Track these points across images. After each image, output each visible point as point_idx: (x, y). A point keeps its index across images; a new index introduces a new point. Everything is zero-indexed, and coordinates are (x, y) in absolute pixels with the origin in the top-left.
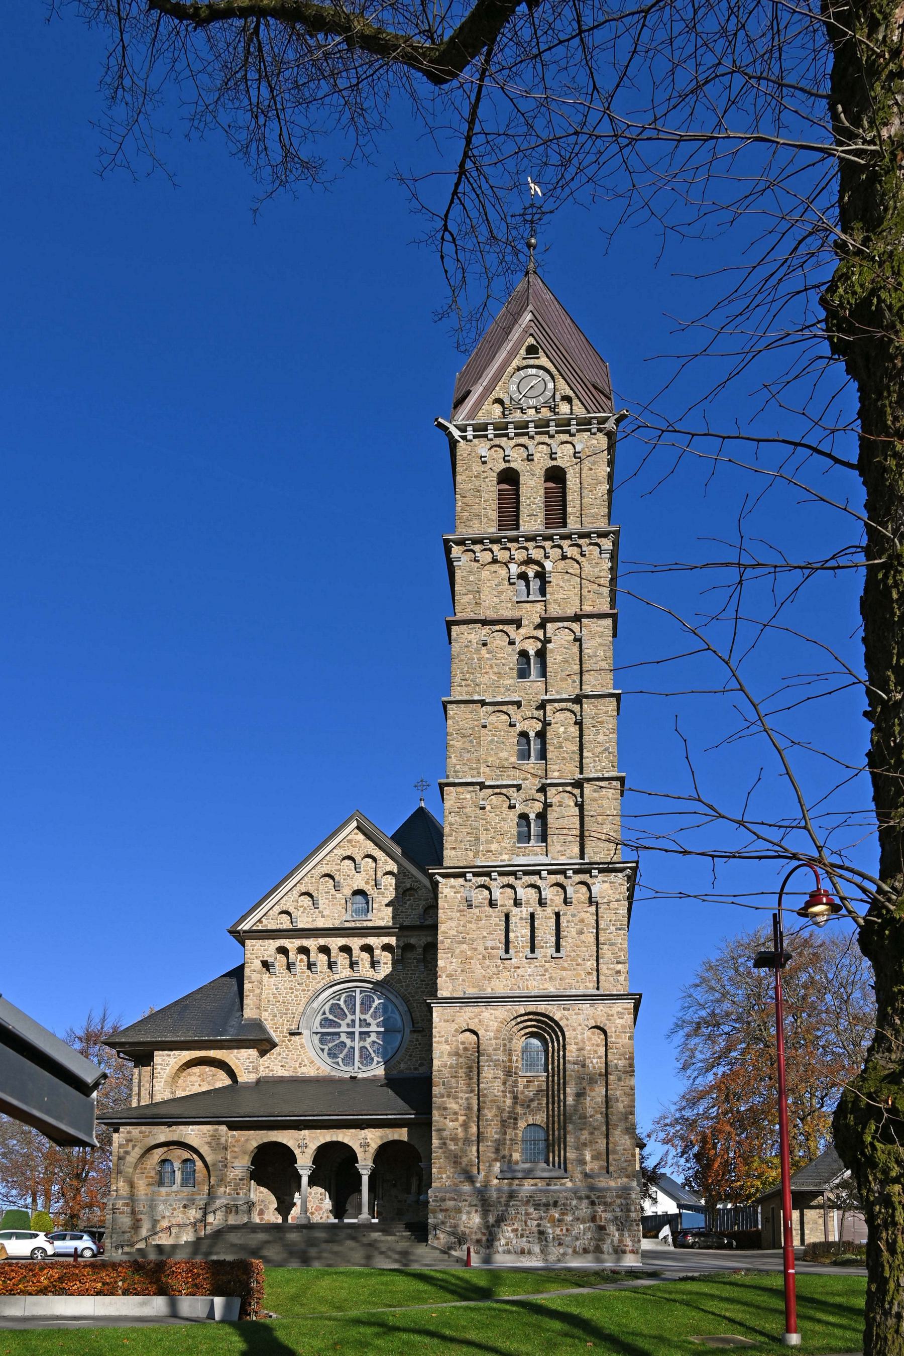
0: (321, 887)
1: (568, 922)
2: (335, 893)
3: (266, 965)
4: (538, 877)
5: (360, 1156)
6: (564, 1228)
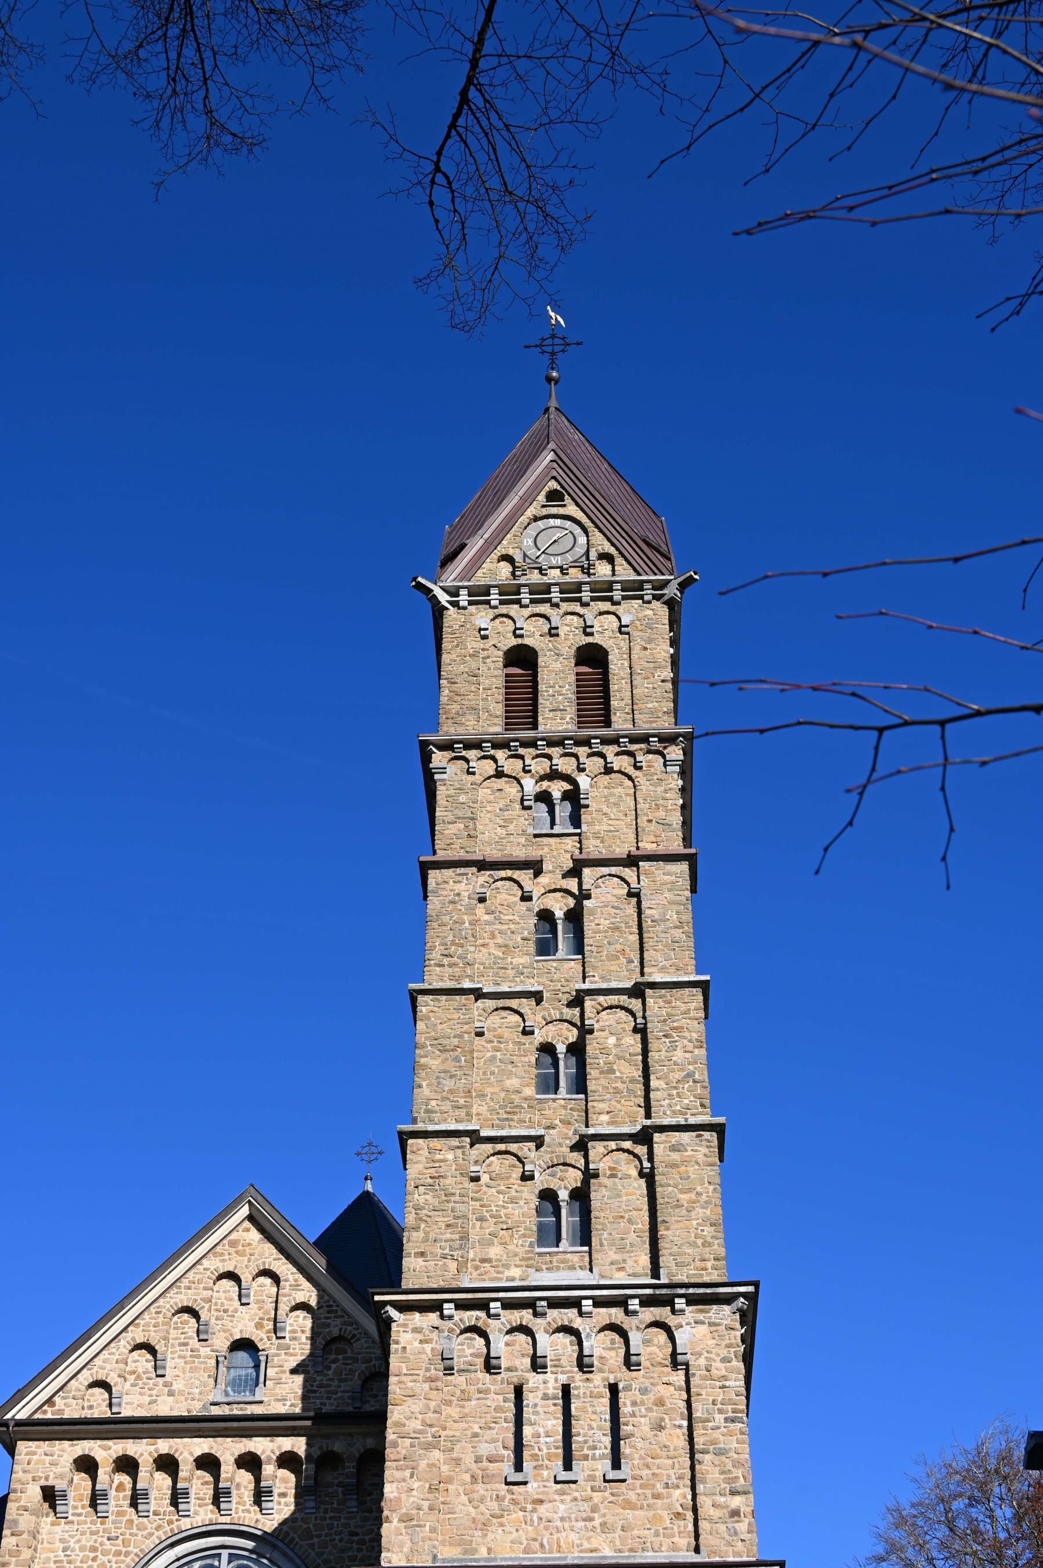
1: (634, 1404)
3: (50, 1495)
4: (575, 1311)
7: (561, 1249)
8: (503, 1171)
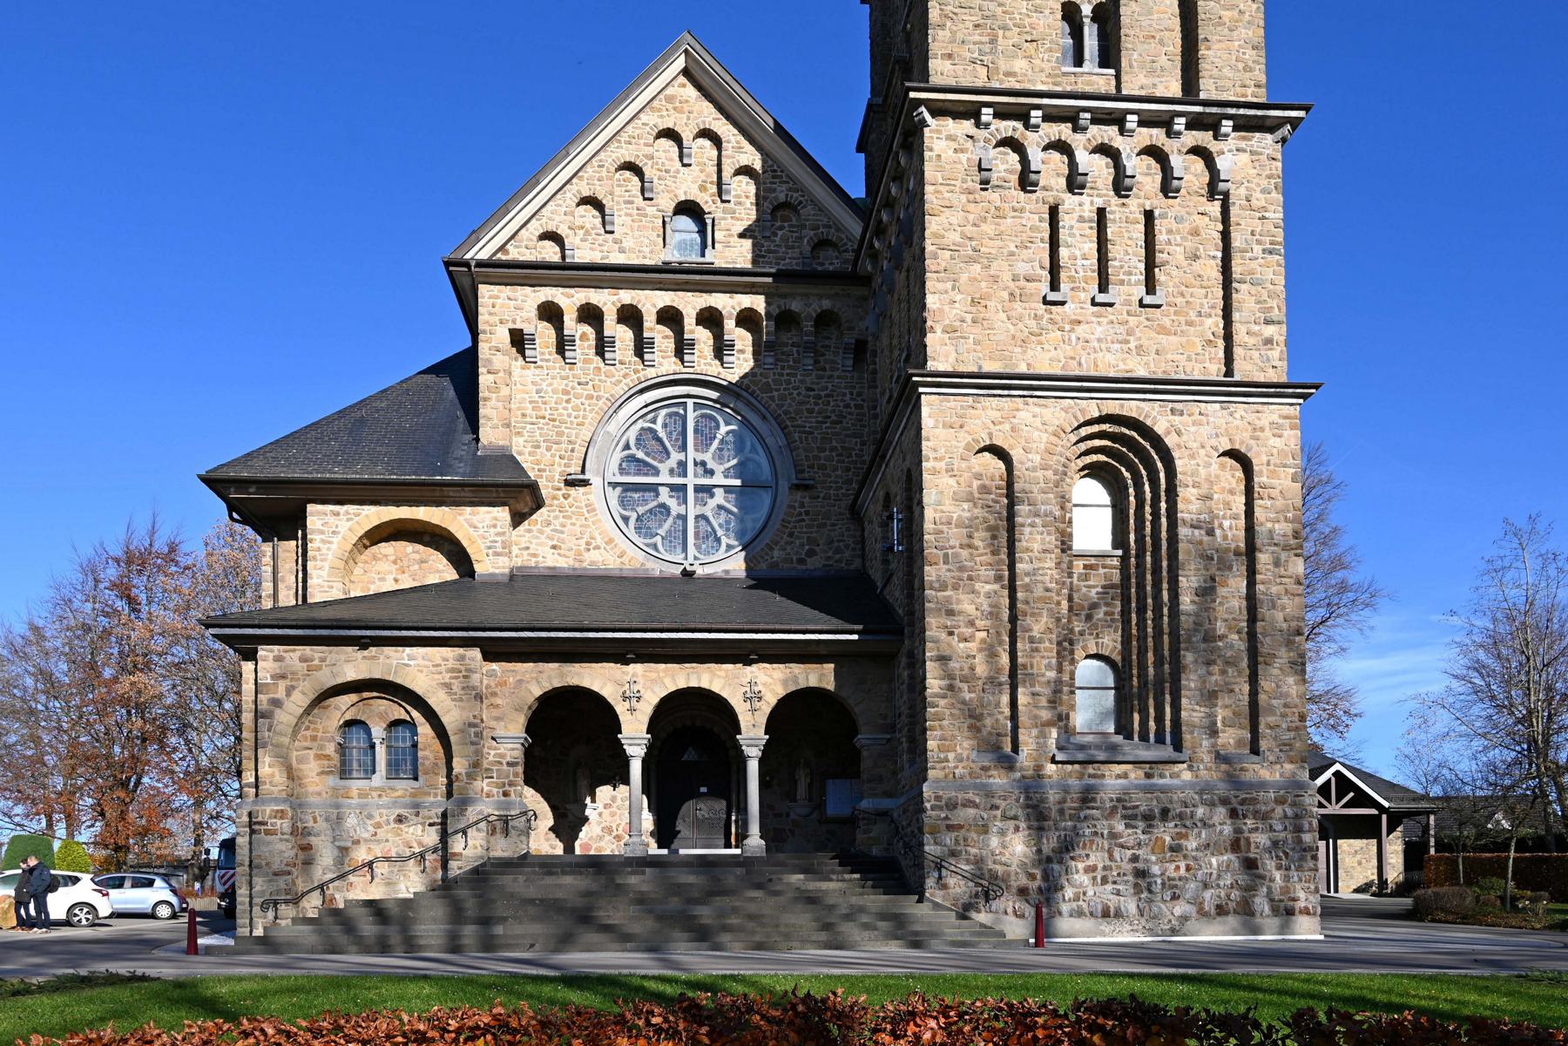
0: (617, 191)
1: (1170, 232)
2: (643, 204)
3: (519, 340)
4: (1116, 128)
5: (744, 719)
6: (1182, 865)
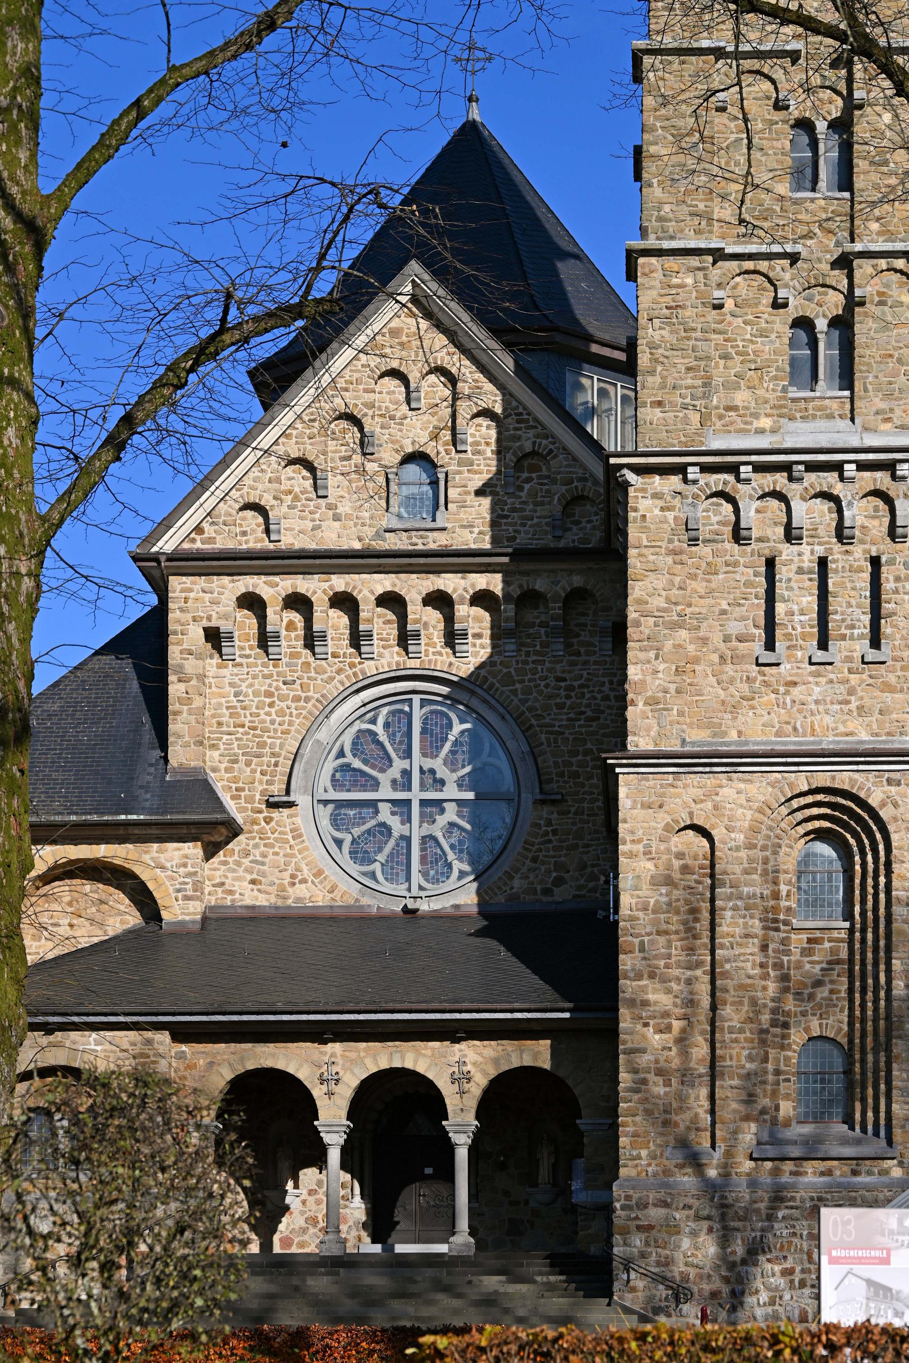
3: (215, 637)
4: (835, 475)
7: (818, 394)
8: (751, 295)
